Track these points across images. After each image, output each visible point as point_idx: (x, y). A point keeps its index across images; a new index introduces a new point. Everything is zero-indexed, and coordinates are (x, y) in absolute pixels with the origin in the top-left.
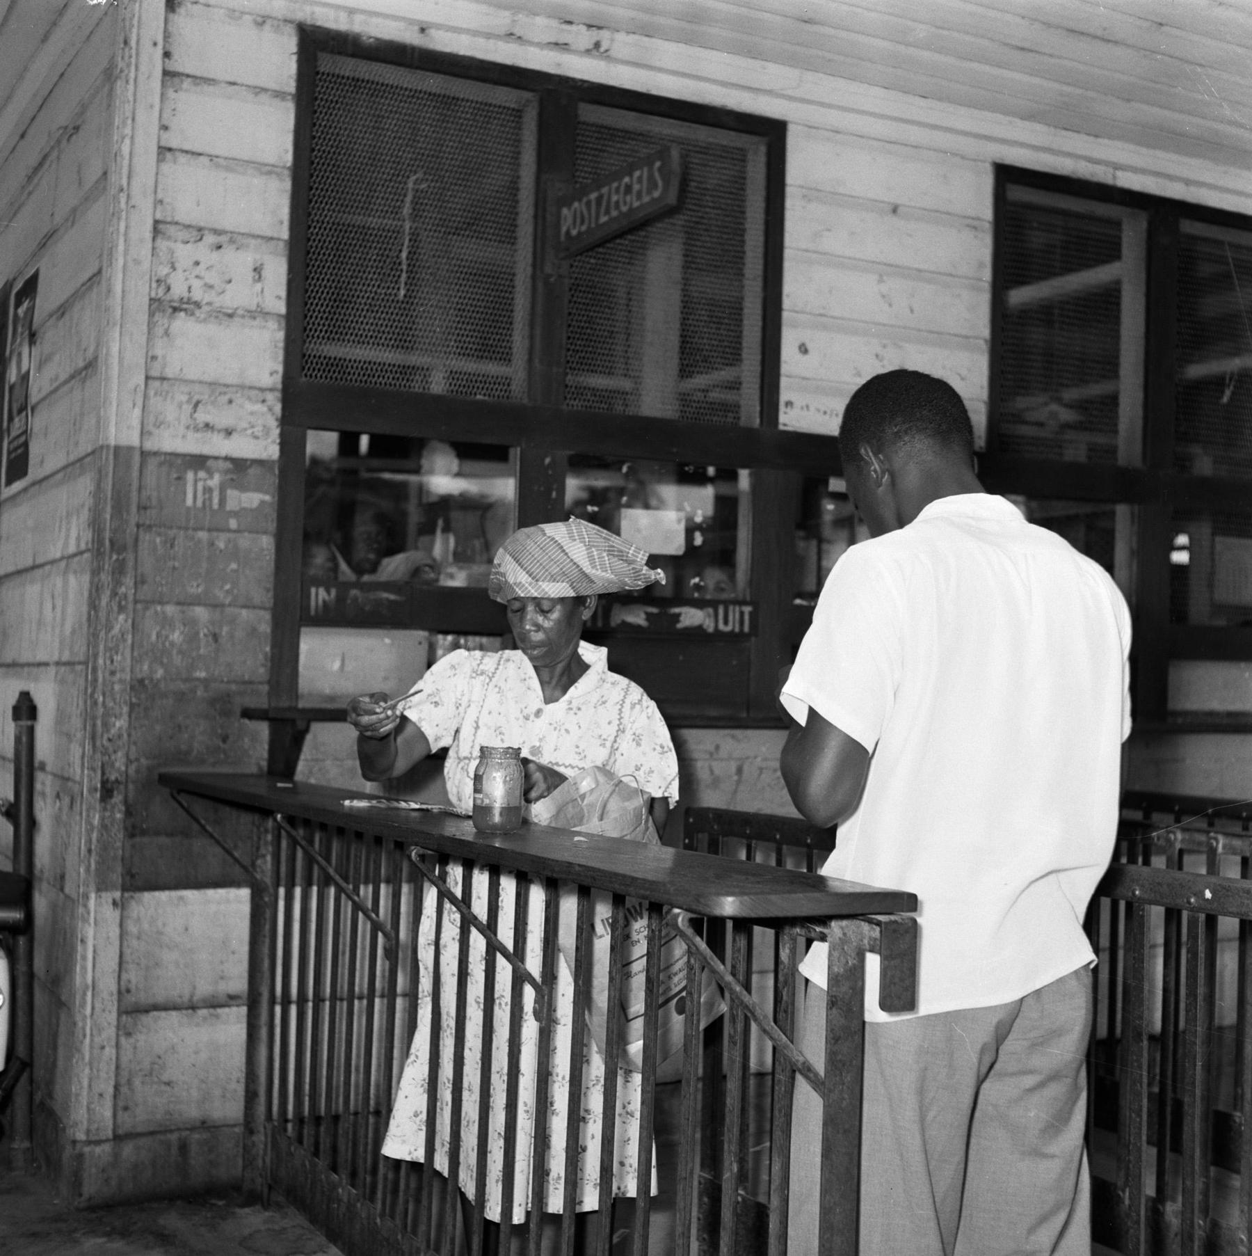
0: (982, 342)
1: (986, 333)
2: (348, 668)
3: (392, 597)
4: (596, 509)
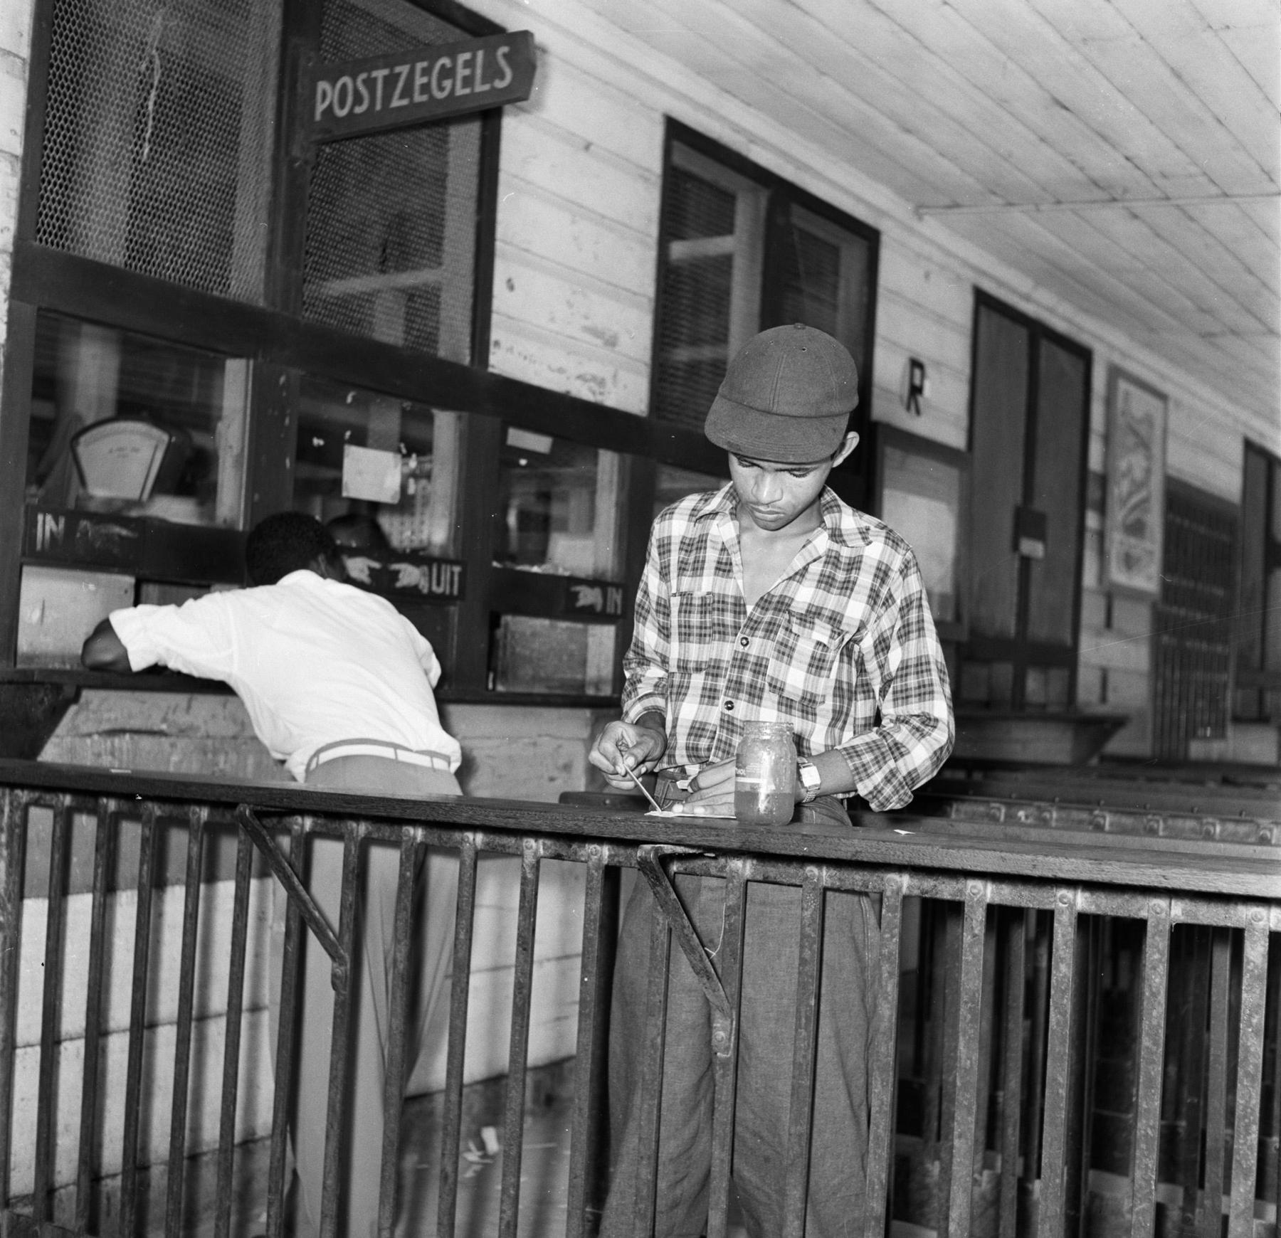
0: (645, 301)
2: (48, 620)
3: (124, 532)
4: (321, 442)
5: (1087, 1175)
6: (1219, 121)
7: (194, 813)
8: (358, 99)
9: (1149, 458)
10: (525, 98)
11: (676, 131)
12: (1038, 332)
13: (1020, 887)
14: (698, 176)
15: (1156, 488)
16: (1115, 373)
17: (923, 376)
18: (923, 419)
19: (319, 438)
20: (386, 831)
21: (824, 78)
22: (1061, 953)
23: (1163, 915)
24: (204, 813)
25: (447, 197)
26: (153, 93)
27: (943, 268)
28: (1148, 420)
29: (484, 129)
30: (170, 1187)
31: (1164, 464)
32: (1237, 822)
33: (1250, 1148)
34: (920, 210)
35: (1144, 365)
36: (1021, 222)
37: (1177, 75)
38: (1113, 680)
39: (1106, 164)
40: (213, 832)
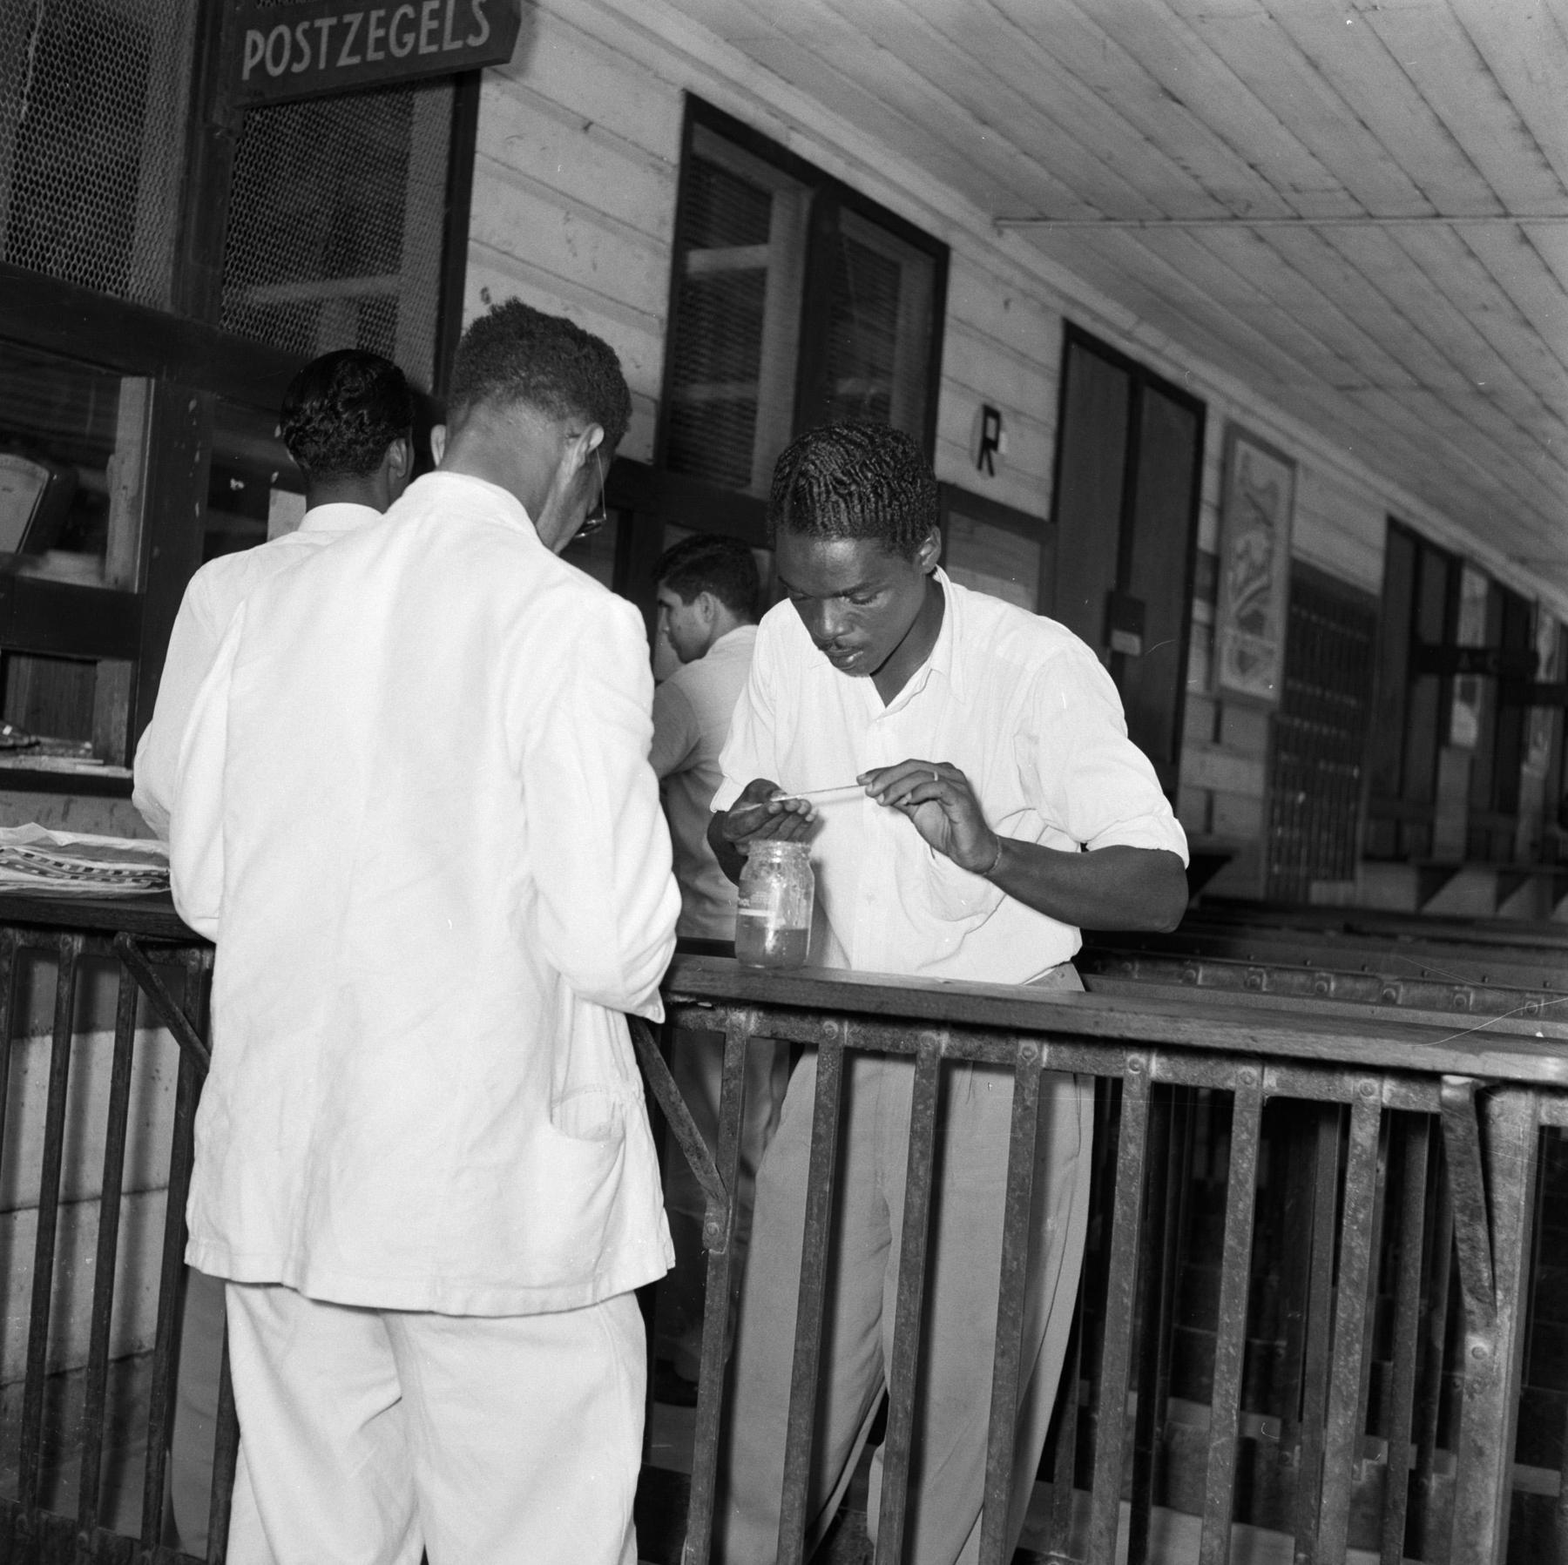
0: (656, 321)
1: (662, 309)
4: (241, 485)
5: (1164, 1404)
6: (1363, 123)
7: (66, 944)
8: (297, 55)
9: (1271, 537)
10: (506, 61)
11: (698, 111)
12: (1140, 378)
13: (1083, 1050)
14: (726, 168)
15: (1279, 572)
16: (1233, 431)
17: (998, 429)
18: (997, 479)
19: (237, 479)
20: (886, 1036)
21: (883, 52)
22: (1130, 1131)
23: (1254, 1086)
24: (78, 943)
25: (409, 183)
26: (35, 35)
27: (1026, 295)
28: (1272, 489)
29: (457, 98)
30: (27, 1410)
31: (1290, 546)
32: (1356, 977)
33: (1352, 1371)
34: (1000, 221)
35: (1269, 424)
36: (1120, 237)
37: (1314, 65)
38: (1221, 806)
39: (1226, 175)
40: (84, 973)
